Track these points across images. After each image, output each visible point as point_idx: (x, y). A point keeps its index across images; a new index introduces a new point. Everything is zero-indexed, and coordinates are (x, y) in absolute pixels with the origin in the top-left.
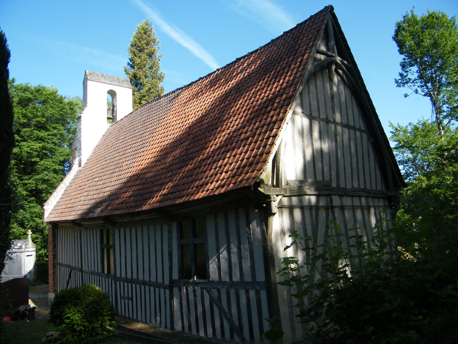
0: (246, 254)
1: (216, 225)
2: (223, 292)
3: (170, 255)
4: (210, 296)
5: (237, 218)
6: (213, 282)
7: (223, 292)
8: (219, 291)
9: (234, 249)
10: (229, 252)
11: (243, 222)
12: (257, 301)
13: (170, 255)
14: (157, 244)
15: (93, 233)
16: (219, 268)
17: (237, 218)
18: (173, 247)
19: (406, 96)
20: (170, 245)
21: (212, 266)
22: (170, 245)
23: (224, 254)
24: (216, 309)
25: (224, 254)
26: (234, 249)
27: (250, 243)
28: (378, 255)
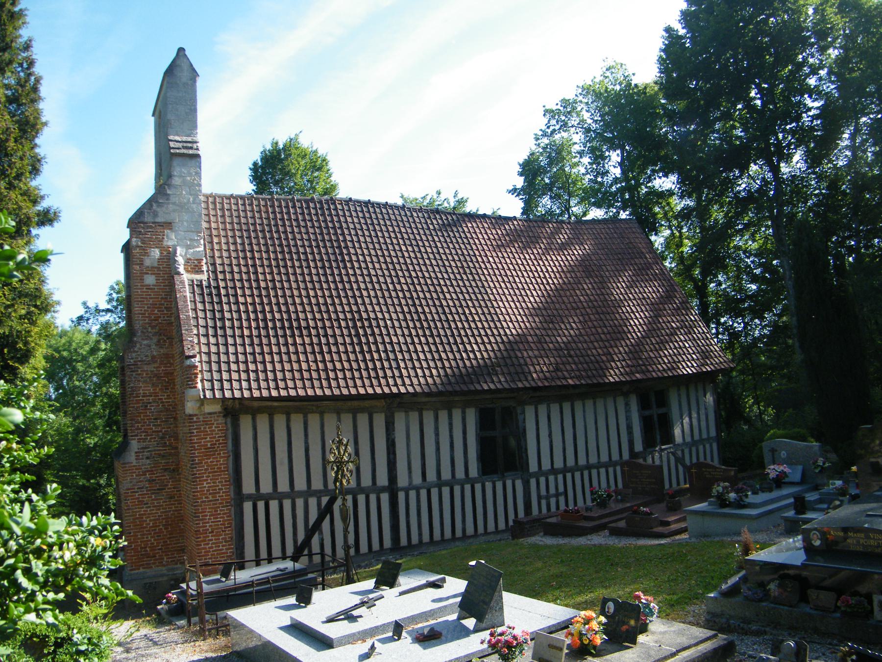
0: (703, 417)
1: (679, 395)
2: (687, 451)
3: (629, 428)
4: (676, 457)
5: (697, 391)
6: (678, 445)
7: (687, 451)
8: (683, 451)
9: (694, 415)
10: (690, 418)
11: (701, 393)
12: (289, 610)
13: (629, 428)
14: (609, 419)
15: (680, 405)
16: (683, 431)
17: (697, 391)
18: (398, 452)
19: (634, 74)
20: (628, 418)
21: (677, 432)
22: (628, 418)
23: (686, 420)
24: (681, 469)
25: (686, 420)
26: (694, 415)
27: (706, 409)
28: (91, 584)
